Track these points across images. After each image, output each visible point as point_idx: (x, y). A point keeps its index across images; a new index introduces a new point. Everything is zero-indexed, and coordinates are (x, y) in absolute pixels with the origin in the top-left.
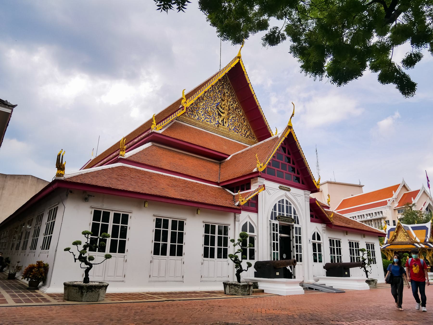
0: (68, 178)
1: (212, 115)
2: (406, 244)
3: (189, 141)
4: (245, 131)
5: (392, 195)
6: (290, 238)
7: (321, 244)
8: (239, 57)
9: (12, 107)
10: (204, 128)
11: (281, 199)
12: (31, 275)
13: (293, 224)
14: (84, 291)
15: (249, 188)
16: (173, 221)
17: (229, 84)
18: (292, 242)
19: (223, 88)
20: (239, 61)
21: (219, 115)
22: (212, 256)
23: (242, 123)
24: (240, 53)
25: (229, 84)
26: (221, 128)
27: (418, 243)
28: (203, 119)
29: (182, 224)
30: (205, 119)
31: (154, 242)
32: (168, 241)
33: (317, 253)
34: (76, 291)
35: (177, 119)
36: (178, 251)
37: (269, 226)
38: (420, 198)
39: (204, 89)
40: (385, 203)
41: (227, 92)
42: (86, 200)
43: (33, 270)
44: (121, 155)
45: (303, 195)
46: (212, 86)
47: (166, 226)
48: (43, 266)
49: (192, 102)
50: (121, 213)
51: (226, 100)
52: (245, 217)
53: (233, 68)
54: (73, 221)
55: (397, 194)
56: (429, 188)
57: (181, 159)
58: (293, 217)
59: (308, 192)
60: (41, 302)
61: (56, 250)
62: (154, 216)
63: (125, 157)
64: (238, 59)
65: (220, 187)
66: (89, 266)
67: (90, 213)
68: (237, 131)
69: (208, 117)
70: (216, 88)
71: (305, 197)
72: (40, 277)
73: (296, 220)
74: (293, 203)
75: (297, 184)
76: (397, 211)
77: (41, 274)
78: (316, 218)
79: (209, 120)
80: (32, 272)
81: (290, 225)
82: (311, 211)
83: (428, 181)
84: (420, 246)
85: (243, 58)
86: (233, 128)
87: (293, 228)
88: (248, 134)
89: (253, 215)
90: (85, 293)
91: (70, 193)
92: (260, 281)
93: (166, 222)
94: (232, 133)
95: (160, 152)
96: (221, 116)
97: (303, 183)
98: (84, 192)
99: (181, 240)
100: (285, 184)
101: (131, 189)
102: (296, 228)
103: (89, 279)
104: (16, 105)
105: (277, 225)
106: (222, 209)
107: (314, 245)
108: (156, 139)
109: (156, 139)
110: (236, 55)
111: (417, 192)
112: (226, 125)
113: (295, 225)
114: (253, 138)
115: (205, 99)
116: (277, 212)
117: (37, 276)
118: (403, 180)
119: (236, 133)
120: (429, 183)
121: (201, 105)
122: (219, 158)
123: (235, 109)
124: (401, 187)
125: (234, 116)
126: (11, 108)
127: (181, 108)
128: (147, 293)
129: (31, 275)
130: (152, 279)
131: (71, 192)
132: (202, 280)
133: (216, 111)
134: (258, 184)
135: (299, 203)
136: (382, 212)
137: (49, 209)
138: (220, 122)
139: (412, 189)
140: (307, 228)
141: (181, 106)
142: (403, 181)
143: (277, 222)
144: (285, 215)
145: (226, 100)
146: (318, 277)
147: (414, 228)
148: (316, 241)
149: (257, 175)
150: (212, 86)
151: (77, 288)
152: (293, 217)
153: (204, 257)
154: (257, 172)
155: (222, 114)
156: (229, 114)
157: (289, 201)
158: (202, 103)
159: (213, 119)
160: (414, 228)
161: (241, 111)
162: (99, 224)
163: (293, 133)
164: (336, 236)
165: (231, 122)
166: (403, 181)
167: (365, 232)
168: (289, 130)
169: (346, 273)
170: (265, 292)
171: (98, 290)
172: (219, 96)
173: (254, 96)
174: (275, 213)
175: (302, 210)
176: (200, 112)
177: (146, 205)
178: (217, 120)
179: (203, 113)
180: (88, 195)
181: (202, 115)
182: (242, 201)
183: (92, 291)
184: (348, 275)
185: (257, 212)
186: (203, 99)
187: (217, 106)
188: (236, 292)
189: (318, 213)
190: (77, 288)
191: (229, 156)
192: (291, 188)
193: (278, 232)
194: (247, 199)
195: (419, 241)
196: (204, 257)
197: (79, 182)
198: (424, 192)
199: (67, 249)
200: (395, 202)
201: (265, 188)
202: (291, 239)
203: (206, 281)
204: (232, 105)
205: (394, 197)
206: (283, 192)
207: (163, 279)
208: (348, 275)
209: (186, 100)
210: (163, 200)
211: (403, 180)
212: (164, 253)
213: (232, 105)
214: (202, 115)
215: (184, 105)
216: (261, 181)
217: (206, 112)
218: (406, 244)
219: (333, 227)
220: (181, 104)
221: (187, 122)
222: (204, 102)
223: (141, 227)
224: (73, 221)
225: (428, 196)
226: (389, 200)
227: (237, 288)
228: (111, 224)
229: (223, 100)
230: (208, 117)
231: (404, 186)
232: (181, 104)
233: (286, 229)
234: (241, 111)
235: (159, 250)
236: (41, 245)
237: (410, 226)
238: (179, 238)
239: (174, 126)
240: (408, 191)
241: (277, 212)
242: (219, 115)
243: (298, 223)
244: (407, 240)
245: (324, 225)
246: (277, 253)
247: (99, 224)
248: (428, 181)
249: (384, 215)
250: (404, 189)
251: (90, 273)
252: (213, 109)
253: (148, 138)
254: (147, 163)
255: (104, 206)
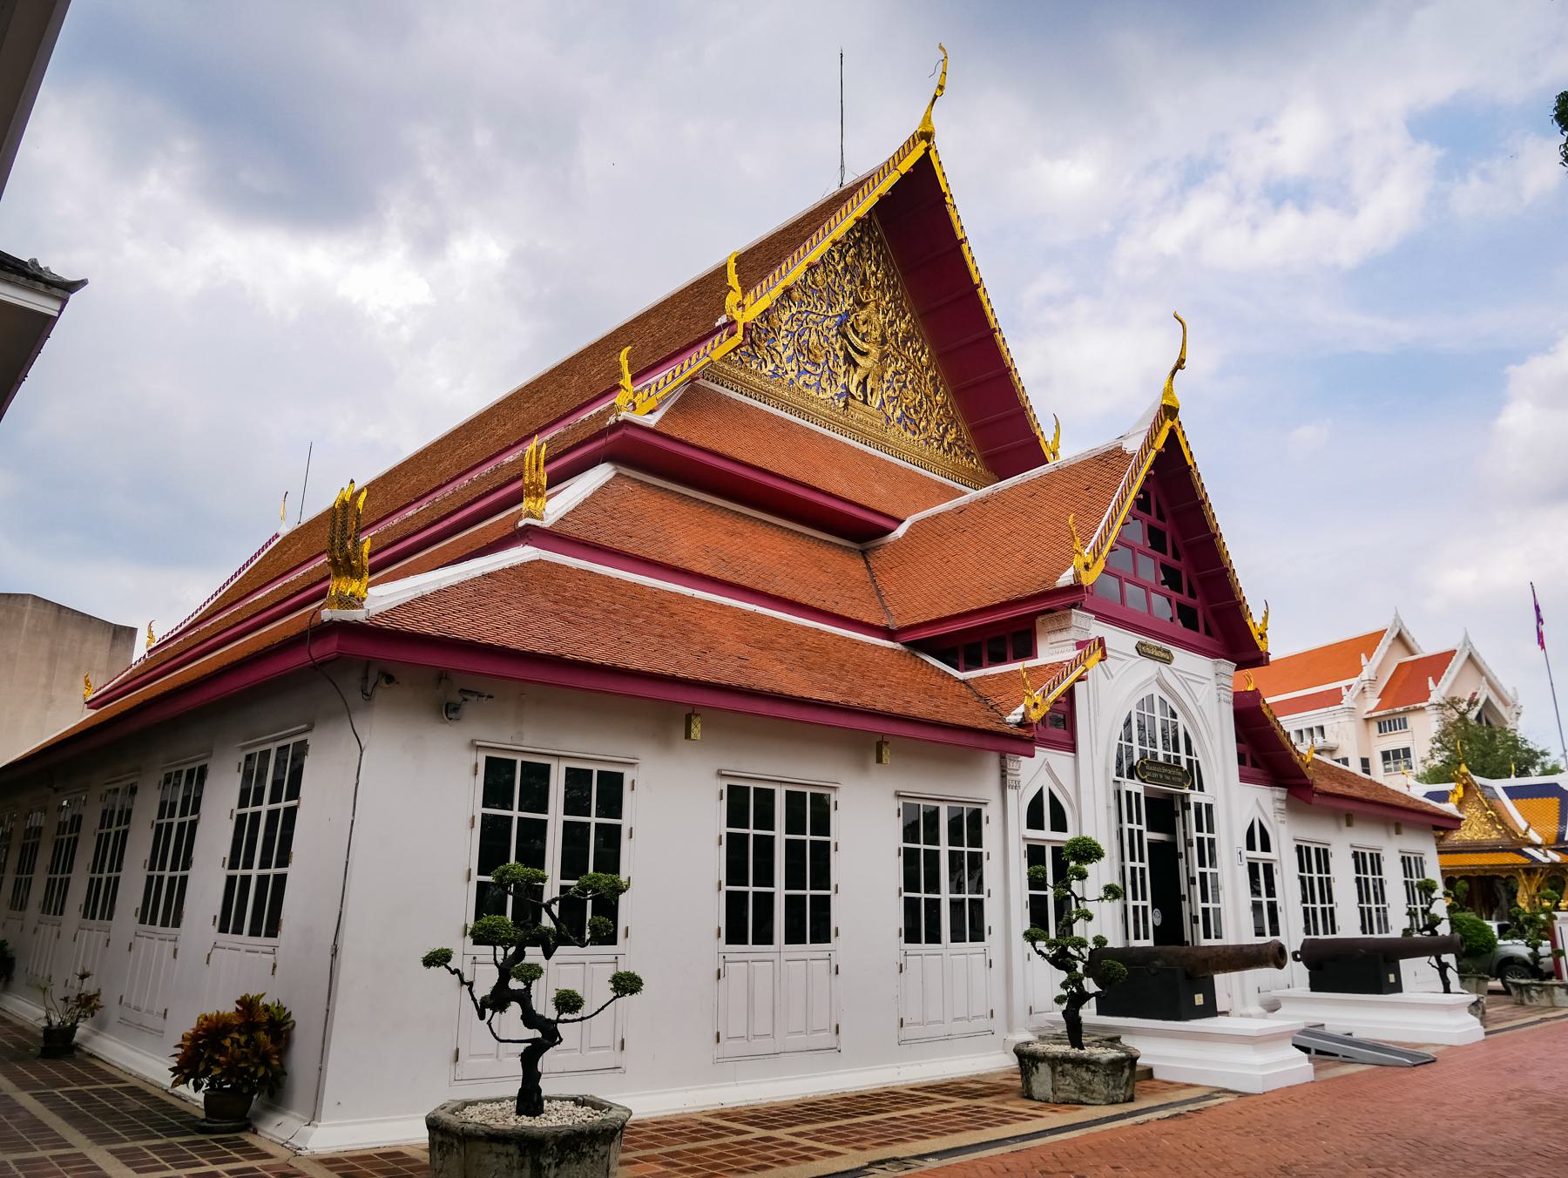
0: (381, 615)
1: (822, 360)
2: (1493, 849)
3: (757, 462)
4: (938, 425)
5: (1357, 670)
6: (1174, 844)
7: (1275, 867)
8: (927, 136)
9: (63, 289)
10: (798, 412)
11: (1144, 694)
12: (218, 1063)
13: (1186, 790)
14: (545, 1161)
15: (1029, 651)
16: (790, 795)
17: (880, 241)
18: (1182, 863)
19: (859, 255)
20: (927, 149)
21: (850, 361)
22: (764, 937)
23: (927, 396)
24: (927, 119)
25: (880, 241)
26: (858, 412)
27: (1536, 846)
28: (792, 375)
29: (612, 787)
30: (798, 377)
31: (476, 878)
32: (775, 887)
33: (1264, 899)
34: (504, 1161)
35: (712, 372)
36: (811, 923)
37: (1113, 803)
38: (1455, 680)
39: (806, 254)
40: (1334, 698)
41: (874, 274)
42: (449, 711)
43: (227, 1042)
44: (530, 515)
45: (1211, 676)
46: (835, 243)
47: (536, 798)
48: (265, 1018)
49: (765, 303)
50: (596, 768)
51: (872, 305)
52: (1036, 771)
53: (905, 178)
54: (393, 815)
55: (1377, 666)
56: (1543, 647)
57: (733, 534)
58: (1184, 765)
59: (1228, 667)
60: (202, 1165)
61: (335, 952)
62: (720, 775)
63: (547, 523)
64: (924, 144)
65: (897, 646)
66: (538, 1034)
67: (469, 769)
68: (912, 427)
69: (808, 367)
70: (836, 256)
71: (1220, 686)
72: (261, 1072)
73: (1192, 777)
74: (1183, 708)
75: (1190, 635)
76: (1374, 727)
77: (265, 1059)
78: (1255, 765)
79: (812, 380)
80: (222, 1050)
81: (1172, 795)
82: (1238, 740)
83: (1540, 620)
84: (1546, 855)
85: (939, 141)
86: (898, 413)
87: (1186, 806)
88: (950, 438)
89: (1059, 760)
90: (553, 1172)
91: (383, 683)
92: (1130, 1031)
93: (537, 775)
94: (894, 433)
95: (654, 503)
96: (856, 365)
97: (1208, 632)
98: (442, 677)
99: (822, 877)
100: (1157, 639)
101: (636, 664)
102: (1198, 806)
103: (540, 1090)
104: (83, 283)
105: (1138, 795)
106: (939, 736)
107: (1253, 868)
108: (635, 452)
109: (635, 452)
110: (915, 126)
111: (1447, 657)
112: (875, 401)
113: (1195, 797)
114: (967, 455)
115: (795, 294)
116: (1136, 744)
117: (246, 1070)
118: (1397, 615)
119: (909, 435)
120: (1543, 628)
121: (785, 318)
122: (858, 531)
123: (904, 343)
124: (1389, 641)
125: (901, 365)
126: (56, 291)
127: (725, 325)
128: (722, 1115)
129: (218, 1063)
130: (728, 1047)
131: (390, 679)
132: (906, 1035)
133: (837, 346)
134: (1074, 635)
135: (1200, 709)
136: (1321, 729)
137: (244, 748)
138: (853, 389)
139: (1427, 647)
140: (1233, 801)
141: (722, 320)
142: (1397, 619)
143: (1136, 786)
144: (1161, 759)
145: (872, 305)
146: (1275, 993)
147: (1512, 792)
148: (1258, 853)
149: (1075, 595)
150: (835, 243)
151: (512, 1149)
152: (1184, 765)
153: (906, 941)
154: (1076, 588)
155: (859, 360)
156: (884, 356)
157: (1170, 702)
158: (788, 314)
159: (826, 376)
160: (1512, 792)
161: (922, 348)
162: (597, 825)
163: (1179, 435)
164: (1318, 833)
165: (890, 392)
166: (1397, 619)
167: (1402, 815)
168: (1169, 424)
169: (1392, 978)
170: (1157, 1075)
171: (603, 1149)
172: (848, 288)
173: (980, 290)
174: (1130, 755)
175: (1211, 736)
176: (781, 349)
177: (696, 731)
178: (842, 380)
179: (790, 352)
180: (462, 691)
181: (790, 359)
182: (1036, 705)
183: (581, 1157)
184: (1397, 987)
185: (1073, 748)
186: (790, 298)
187: (840, 325)
188: (1082, 1090)
189: (1263, 751)
190: (512, 1149)
191: (901, 522)
192: (1176, 651)
193: (1143, 827)
194: (1051, 698)
195: (1538, 840)
196: (906, 941)
197: (429, 631)
198: (1470, 657)
199: (438, 959)
200: (1368, 694)
201: (1104, 654)
202: (1181, 848)
203: (919, 1040)
204: (891, 323)
205: (1365, 675)
206: (1150, 667)
207: (767, 1045)
208: (1397, 987)
209: (745, 293)
210: (762, 707)
211: (1397, 615)
212: (764, 937)
213: (891, 323)
214: (790, 359)
215: (737, 314)
216: (1086, 625)
217: (803, 350)
218: (1493, 849)
219: (1316, 799)
220: (723, 311)
221: (735, 383)
222: (794, 310)
223: (674, 822)
224: (393, 815)
225: (1481, 672)
226: (1348, 687)
227: (1087, 1076)
228: (556, 817)
229: (863, 305)
230: (808, 367)
231: (1400, 637)
232: (723, 311)
233: (1163, 812)
234: (922, 348)
235: (744, 923)
236: (140, 905)
237: (1498, 785)
238: (813, 865)
239: (692, 398)
240: (1412, 654)
241: (1136, 744)
242: (850, 361)
243: (1201, 789)
244: (1495, 835)
245: (1280, 793)
246: (1145, 908)
247: (597, 825)
248: (1540, 620)
249: (1331, 739)
250: (1400, 649)
251: (547, 1061)
252: (827, 339)
253: (602, 442)
254: (629, 546)
255: (525, 739)
